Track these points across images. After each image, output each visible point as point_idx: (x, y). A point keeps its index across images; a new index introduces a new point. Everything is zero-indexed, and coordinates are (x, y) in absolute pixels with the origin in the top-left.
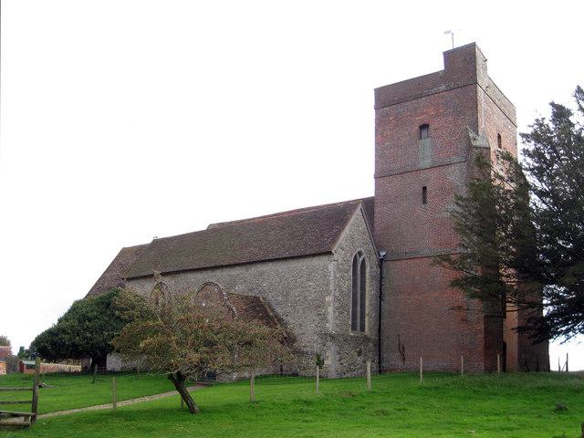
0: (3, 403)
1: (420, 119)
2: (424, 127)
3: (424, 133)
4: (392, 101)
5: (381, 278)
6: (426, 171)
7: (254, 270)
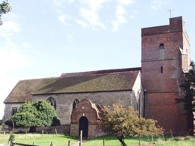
0: (104, 145)
1: (160, 42)
2: (162, 45)
3: (162, 47)
4: (147, 33)
5: (144, 99)
6: (162, 61)
7: (96, 94)
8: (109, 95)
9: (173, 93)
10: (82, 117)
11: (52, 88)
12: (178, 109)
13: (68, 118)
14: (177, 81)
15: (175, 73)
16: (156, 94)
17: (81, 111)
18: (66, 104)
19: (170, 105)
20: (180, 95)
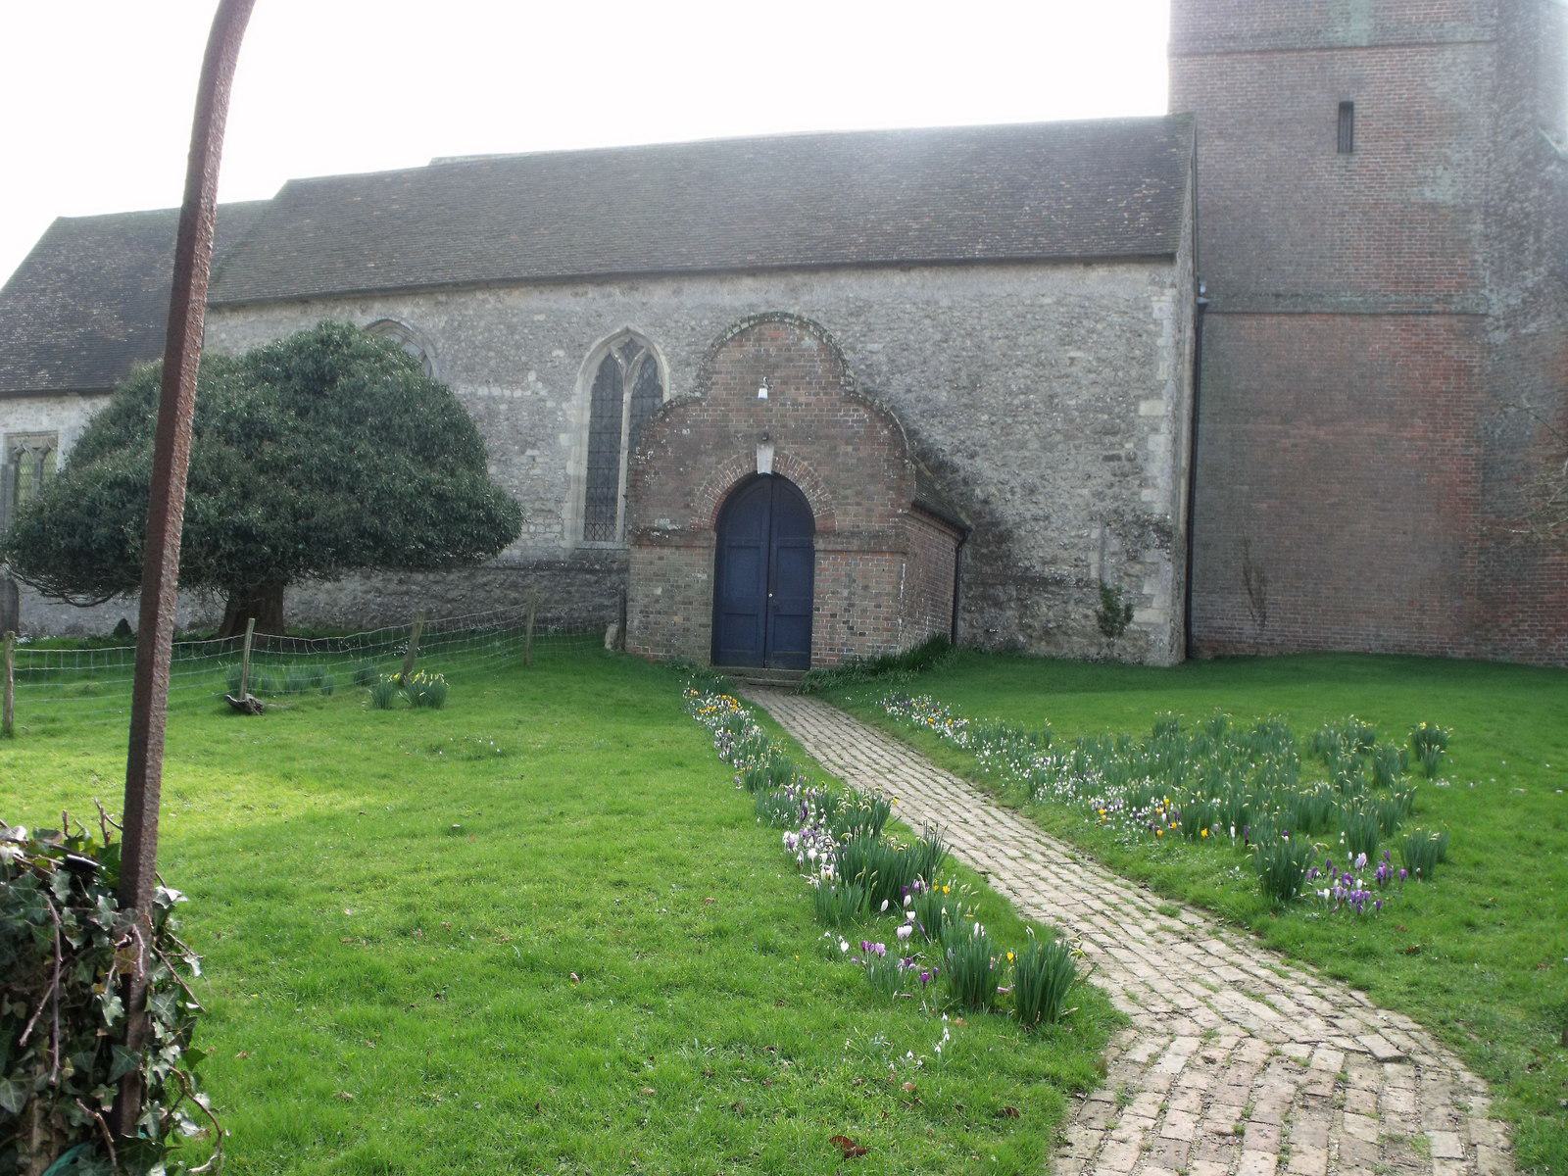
8: (945, 303)
9: (1440, 320)
10: (753, 479)
11: (347, 802)
12: (1474, 450)
13: (551, 505)
14: (1478, 227)
15: (1456, 157)
16: (1288, 324)
17: (739, 424)
18: (532, 377)
19: (1413, 413)
20: (1500, 337)
